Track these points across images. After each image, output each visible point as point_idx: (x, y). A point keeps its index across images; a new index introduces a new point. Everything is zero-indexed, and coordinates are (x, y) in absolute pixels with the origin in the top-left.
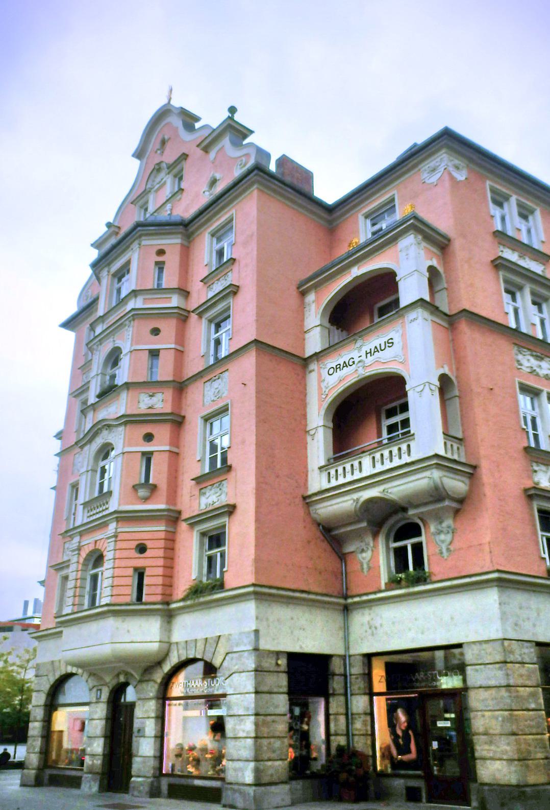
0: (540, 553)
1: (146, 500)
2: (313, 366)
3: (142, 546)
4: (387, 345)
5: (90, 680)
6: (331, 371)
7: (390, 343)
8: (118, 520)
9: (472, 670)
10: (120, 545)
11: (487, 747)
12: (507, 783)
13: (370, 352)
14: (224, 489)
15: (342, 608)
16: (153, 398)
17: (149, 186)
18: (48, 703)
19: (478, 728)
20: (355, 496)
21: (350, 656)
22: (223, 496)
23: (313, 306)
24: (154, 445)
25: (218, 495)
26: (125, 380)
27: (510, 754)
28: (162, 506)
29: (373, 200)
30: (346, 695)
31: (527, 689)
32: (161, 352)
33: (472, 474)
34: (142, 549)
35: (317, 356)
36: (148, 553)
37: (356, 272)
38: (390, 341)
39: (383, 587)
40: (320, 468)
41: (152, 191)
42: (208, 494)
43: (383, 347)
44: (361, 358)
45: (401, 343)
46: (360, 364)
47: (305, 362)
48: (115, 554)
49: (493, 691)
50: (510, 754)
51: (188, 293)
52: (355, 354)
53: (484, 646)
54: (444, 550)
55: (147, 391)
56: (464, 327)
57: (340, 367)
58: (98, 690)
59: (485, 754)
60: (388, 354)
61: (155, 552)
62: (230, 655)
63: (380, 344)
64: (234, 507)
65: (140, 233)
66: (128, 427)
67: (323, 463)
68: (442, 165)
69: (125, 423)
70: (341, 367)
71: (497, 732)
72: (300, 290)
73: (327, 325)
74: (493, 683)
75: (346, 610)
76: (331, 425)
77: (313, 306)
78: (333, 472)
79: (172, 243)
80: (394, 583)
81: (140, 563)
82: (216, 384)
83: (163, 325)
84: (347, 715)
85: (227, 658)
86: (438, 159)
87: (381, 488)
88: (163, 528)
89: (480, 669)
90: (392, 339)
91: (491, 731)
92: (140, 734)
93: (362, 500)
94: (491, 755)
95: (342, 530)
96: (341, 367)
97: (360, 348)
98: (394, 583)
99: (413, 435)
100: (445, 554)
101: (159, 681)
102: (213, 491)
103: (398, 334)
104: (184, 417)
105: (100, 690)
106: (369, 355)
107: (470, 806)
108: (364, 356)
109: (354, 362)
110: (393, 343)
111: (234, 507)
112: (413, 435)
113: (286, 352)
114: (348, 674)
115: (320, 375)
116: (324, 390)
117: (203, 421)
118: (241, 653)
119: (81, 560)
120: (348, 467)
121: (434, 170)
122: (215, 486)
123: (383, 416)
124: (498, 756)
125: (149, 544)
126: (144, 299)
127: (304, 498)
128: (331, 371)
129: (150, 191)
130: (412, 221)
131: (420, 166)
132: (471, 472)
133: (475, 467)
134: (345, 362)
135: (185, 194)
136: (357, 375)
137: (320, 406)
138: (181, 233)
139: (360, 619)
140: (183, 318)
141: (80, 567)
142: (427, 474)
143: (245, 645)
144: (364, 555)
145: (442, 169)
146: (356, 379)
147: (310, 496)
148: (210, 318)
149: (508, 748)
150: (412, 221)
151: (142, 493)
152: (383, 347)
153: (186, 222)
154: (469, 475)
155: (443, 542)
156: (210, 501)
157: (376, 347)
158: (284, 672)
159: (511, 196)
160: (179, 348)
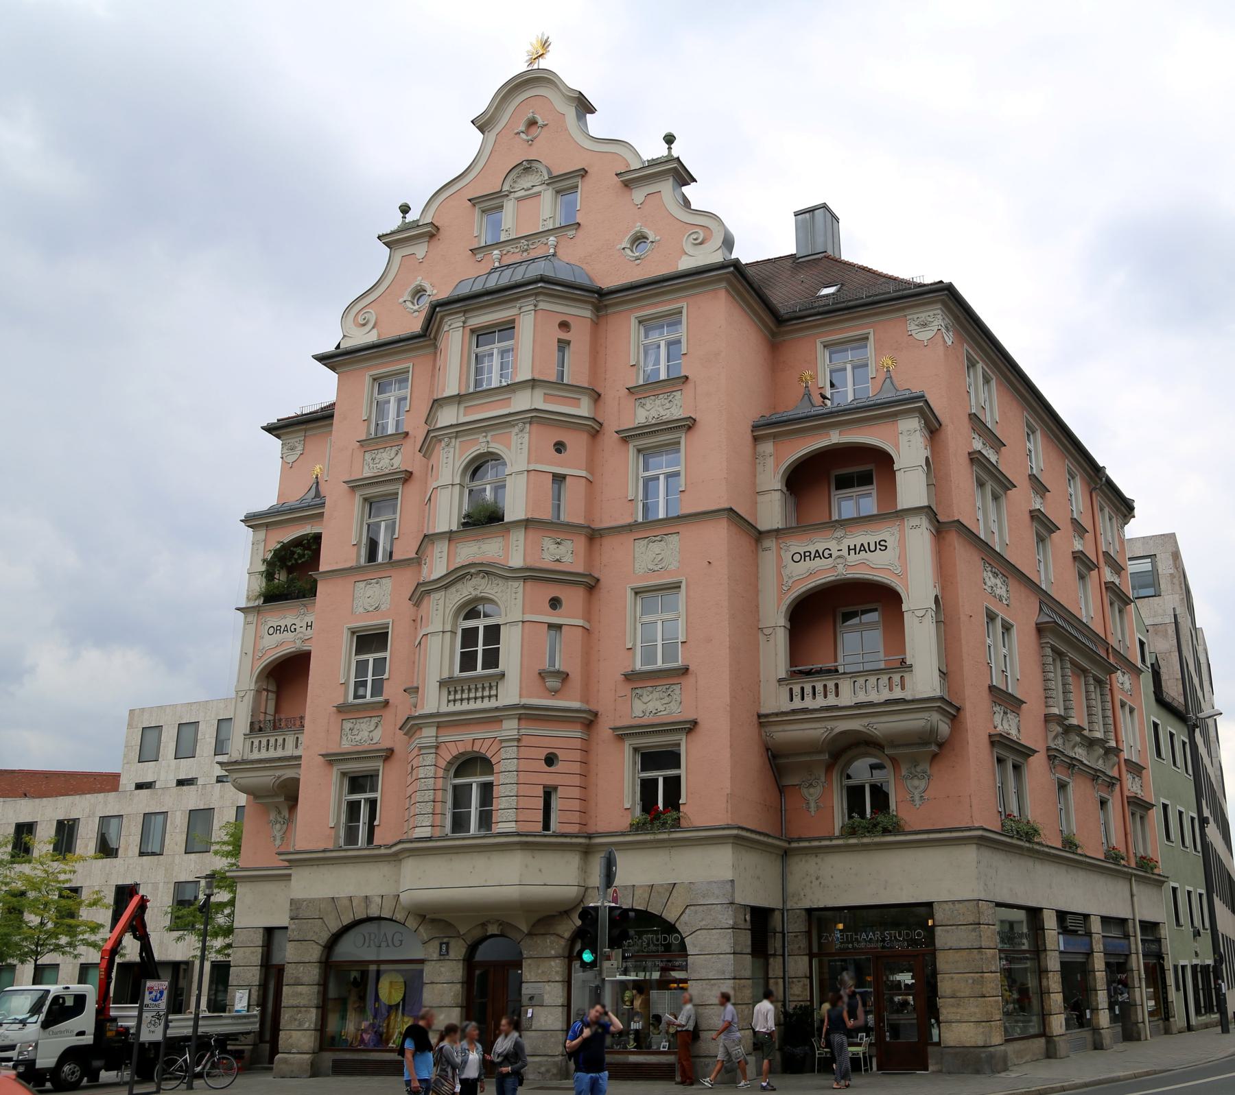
0: (998, 808)
1: (555, 692)
2: (770, 543)
3: (552, 756)
4: (878, 547)
5: (421, 929)
6: (797, 557)
7: (882, 545)
8: (520, 718)
9: (942, 930)
10: (525, 752)
11: (954, 1010)
12: (973, 1044)
13: (855, 549)
14: (676, 696)
15: (781, 853)
16: (560, 547)
17: (506, 188)
18: (324, 959)
19: (945, 992)
20: (830, 725)
21: (788, 910)
22: (674, 707)
23: (770, 462)
24: (559, 616)
25: (664, 702)
26: (521, 516)
27: (978, 1015)
28: (576, 705)
29: (840, 329)
30: (783, 955)
31: (991, 950)
32: (568, 478)
33: (954, 716)
34: (550, 760)
35: (777, 533)
36: (559, 767)
37: (835, 437)
38: (882, 543)
39: (837, 833)
40: (780, 681)
41: (512, 195)
42: (645, 699)
43: (872, 548)
44: (840, 553)
45: (897, 551)
46: (839, 560)
47: (760, 537)
48: (518, 764)
49: (965, 953)
50: (978, 1015)
51: (599, 395)
52: (833, 545)
53: (957, 905)
54: (917, 798)
55: (554, 536)
56: (955, 542)
57: (810, 556)
58: (441, 944)
59: (951, 1017)
60: (878, 558)
61: (568, 765)
62: (689, 907)
63: (869, 543)
64: (695, 723)
65: (540, 290)
66: (529, 584)
67: (783, 674)
68: (936, 323)
69: (525, 579)
70: (812, 556)
71: (967, 994)
72: (755, 434)
73: (785, 489)
74: (964, 945)
75: (785, 855)
76: (788, 626)
77: (770, 462)
78: (797, 689)
79: (581, 314)
80: (851, 831)
81: (550, 780)
82: (656, 548)
83: (570, 438)
84: (784, 978)
85: (687, 911)
86: (931, 313)
87: (865, 721)
88: (579, 735)
89: (952, 929)
90: (886, 541)
91: (958, 995)
92: (534, 1002)
93: (837, 730)
94: (958, 1018)
95: (791, 760)
96: (812, 556)
97: (839, 540)
98: (851, 831)
99: (911, 666)
100: (918, 802)
101: (567, 935)
102: (656, 695)
103: (893, 537)
104: (598, 580)
105: (447, 944)
106: (853, 552)
107: (927, 1070)
108: (845, 552)
109: (831, 555)
110: (886, 547)
111: (695, 723)
112: (911, 666)
113: (742, 518)
114: (786, 932)
115: (780, 558)
116: (785, 580)
117: (633, 594)
118: (709, 906)
119: (443, 764)
120: (819, 688)
121: (925, 325)
122: (659, 689)
123: (839, 620)
124: (966, 1018)
125: (561, 754)
126: (545, 394)
127: (759, 716)
128: (797, 557)
129: (507, 196)
130: (921, 404)
131: (907, 312)
132: (955, 713)
133: (958, 709)
134: (817, 551)
135: (581, 232)
136: (836, 574)
137: (780, 600)
138: (592, 303)
139: (803, 868)
140: (594, 432)
141: (441, 773)
142: (926, 715)
143: (717, 897)
144: (812, 790)
145: (936, 328)
146: (833, 578)
147: (767, 716)
148: (639, 447)
149: (977, 1010)
150: (921, 404)
151: (552, 683)
152: (872, 548)
153: (603, 292)
154: (951, 717)
155: (916, 788)
156: (651, 706)
157: (862, 545)
158: (749, 929)
159: (978, 363)
160: (589, 477)
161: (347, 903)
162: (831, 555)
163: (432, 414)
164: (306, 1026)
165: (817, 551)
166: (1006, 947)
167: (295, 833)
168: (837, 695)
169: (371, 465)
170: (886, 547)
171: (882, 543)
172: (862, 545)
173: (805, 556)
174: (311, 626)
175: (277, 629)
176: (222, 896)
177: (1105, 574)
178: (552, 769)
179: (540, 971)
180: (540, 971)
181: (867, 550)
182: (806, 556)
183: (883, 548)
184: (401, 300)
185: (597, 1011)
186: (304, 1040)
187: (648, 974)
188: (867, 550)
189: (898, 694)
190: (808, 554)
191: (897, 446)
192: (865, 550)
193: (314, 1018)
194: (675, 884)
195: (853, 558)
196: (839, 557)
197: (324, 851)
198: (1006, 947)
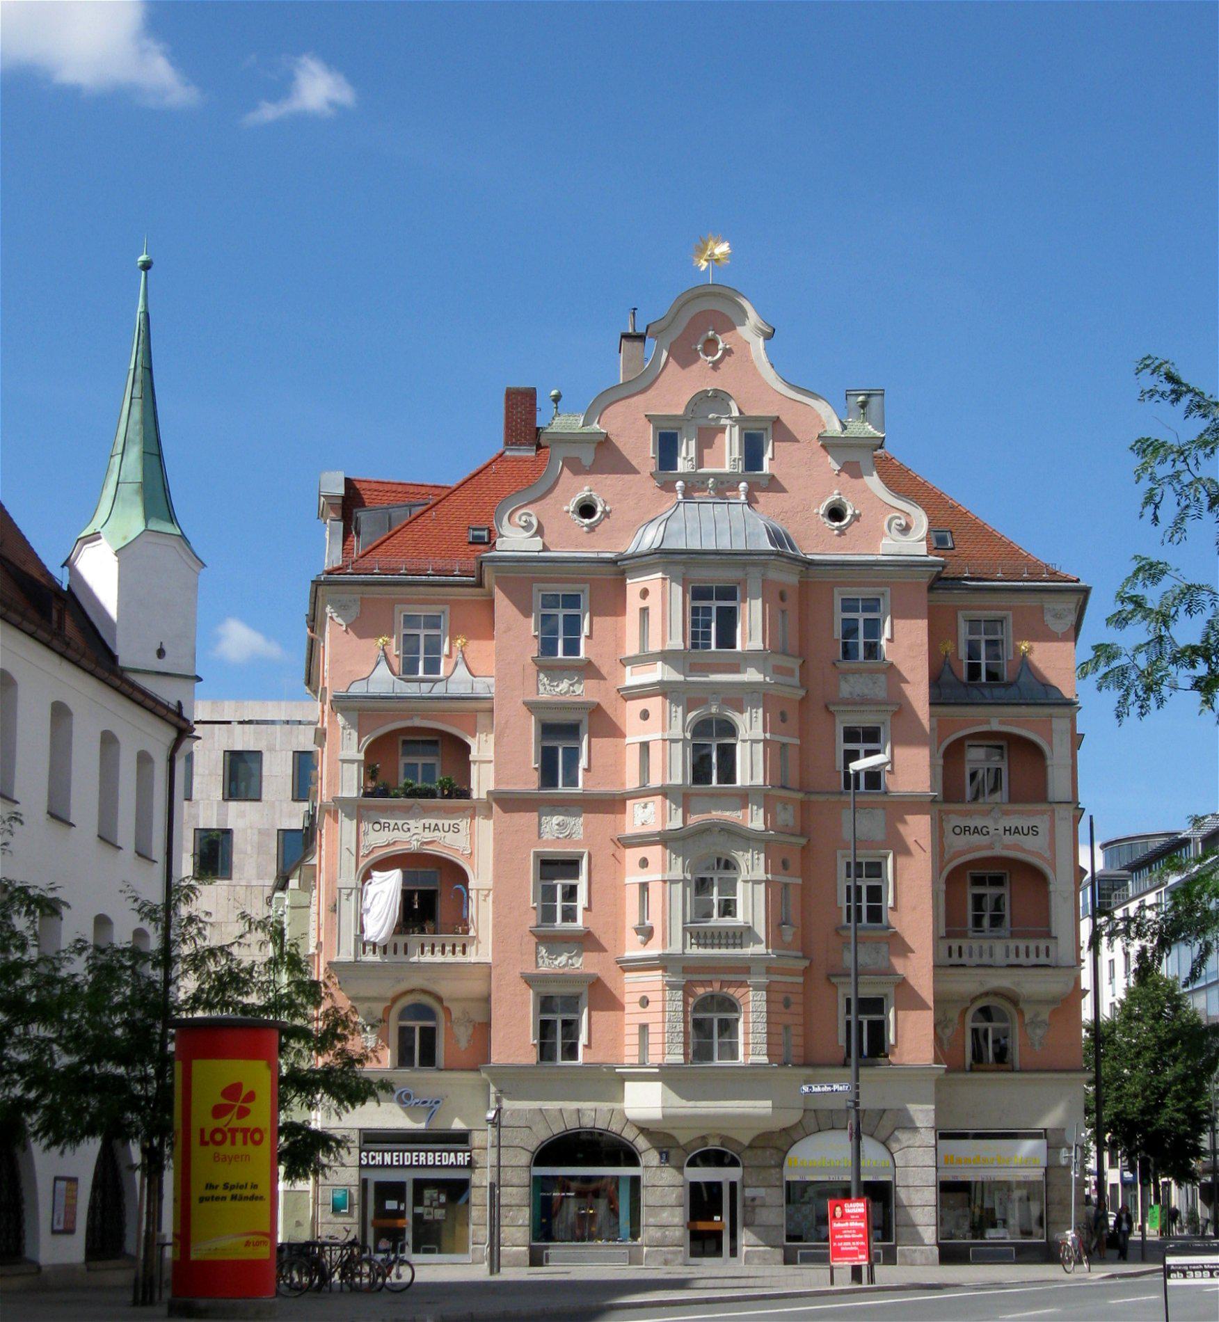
6: (957, 830)
7: (1033, 830)
43: (1026, 832)
96: (391, 828)
97: (996, 821)
128: (957, 830)
134: (976, 827)
152: (1026, 832)
157: (1017, 828)
161: (557, 1113)
162: (988, 832)
163: (635, 795)
166: (192, 895)
172: (1017, 828)
174: (1005, 830)
175: (966, 830)
177: (568, 1207)
182: (966, 830)
185: (87, 1031)
187: (7, 1090)
189: (292, 1189)
191: (1050, 743)
195: (1008, 839)
197: (388, 845)
198: (192, 895)
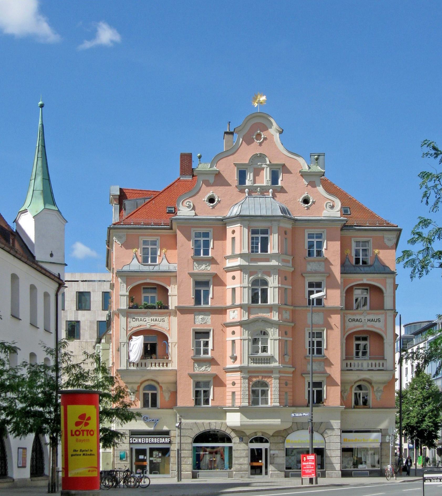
4: (162, 320)
6: (350, 320)
7: (379, 320)
13: (153, 320)
43: (376, 321)
60: (377, 324)
70: (154, 320)
96: (139, 320)
109: (362, 321)
128: (350, 320)
134: (357, 319)
152: (376, 321)
157: (372, 319)
164: (189, 463)
165: (357, 319)
167: (242, 429)
168: (347, 364)
169: (197, 268)
170: (380, 321)
171: (379, 320)
172: (372, 319)
173: (353, 320)
176: (74, 375)
178: (287, 387)
179: (276, 447)
180: (276, 447)
181: (158, 321)
182: (353, 320)
183: (163, 321)
184: (203, 199)
186: (188, 467)
188: (158, 321)
190: (354, 320)
192: (373, 321)
193: (191, 461)
194: (322, 423)
195: (369, 323)
196: (365, 322)
